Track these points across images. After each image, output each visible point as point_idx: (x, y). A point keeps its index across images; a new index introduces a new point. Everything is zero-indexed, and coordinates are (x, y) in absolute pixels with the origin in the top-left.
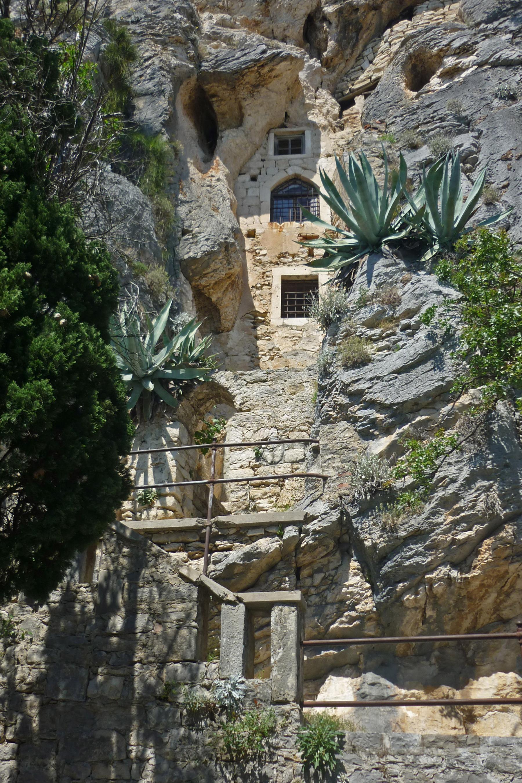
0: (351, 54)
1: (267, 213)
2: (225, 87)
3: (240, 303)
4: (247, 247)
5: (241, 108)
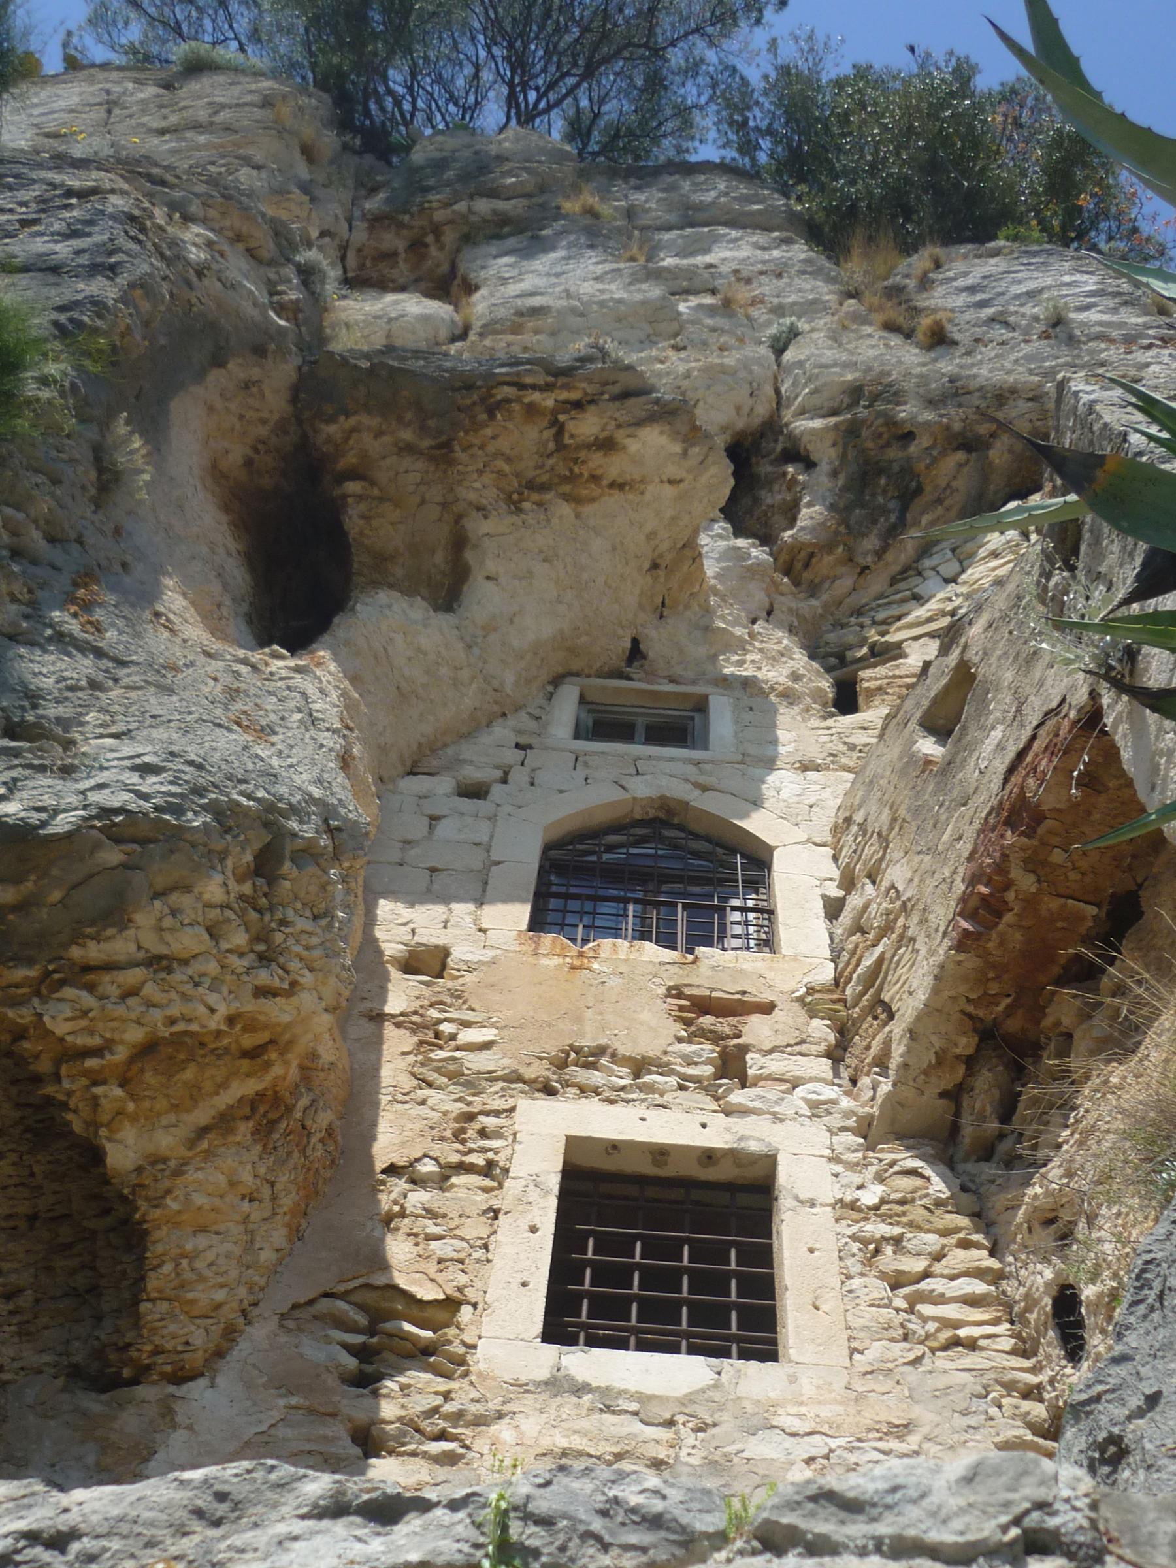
0: (880, 553)
1: (523, 901)
2: (407, 435)
3: (296, 1234)
4: (395, 1003)
5: (459, 542)
